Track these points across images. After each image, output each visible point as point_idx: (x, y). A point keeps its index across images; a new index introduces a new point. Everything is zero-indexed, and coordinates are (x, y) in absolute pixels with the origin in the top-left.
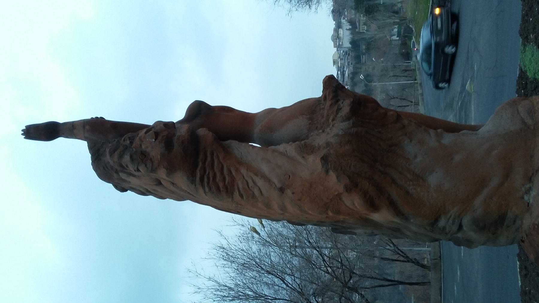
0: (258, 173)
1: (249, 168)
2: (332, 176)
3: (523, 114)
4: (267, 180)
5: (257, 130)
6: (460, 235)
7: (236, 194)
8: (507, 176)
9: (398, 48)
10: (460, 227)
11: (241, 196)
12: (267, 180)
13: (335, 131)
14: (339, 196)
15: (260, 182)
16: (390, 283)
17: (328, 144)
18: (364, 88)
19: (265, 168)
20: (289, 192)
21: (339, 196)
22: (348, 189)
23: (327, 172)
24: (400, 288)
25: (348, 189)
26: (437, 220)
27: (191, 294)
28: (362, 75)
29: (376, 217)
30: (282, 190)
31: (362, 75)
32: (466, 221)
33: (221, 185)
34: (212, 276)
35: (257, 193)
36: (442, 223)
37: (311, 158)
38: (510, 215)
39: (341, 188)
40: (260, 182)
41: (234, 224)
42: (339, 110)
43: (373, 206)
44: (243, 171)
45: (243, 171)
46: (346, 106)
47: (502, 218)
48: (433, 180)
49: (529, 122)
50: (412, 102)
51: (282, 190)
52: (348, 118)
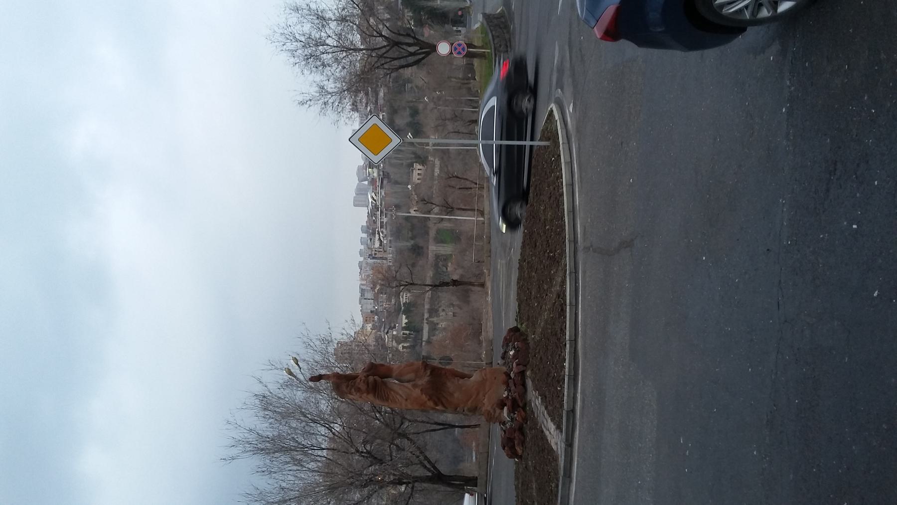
0: (398, 393)
1: (394, 391)
2: (424, 396)
3: (483, 375)
4: (401, 396)
5: (394, 375)
6: (464, 413)
7: (390, 401)
8: (478, 394)
9: (461, 69)
10: (464, 411)
11: (391, 401)
12: (401, 396)
13: (425, 380)
14: (426, 402)
15: (398, 397)
16: (441, 427)
17: (422, 384)
18: (409, 119)
19: (400, 392)
20: (409, 401)
21: (426, 402)
22: (429, 400)
23: (422, 394)
24: (456, 432)
25: (429, 400)
26: (457, 409)
27: (341, 438)
28: (409, 134)
29: (437, 408)
30: (406, 400)
31: (409, 134)
32: (466, 409)
33: (384, 398)
34: (253, 427)
35: (397, 401)
36: (458, 409)
37: (417, 389)
38: (478, 407)
39: (426, 399)
40: (398, 397)
41: (271, 368)
42: (426, 374)
43: (436, 404)
44: (392, 393)
45: (392, 393)
46: (428, 372)
47: (476, 407)
48: (456, 395)
49: (485, 378)
50: (476, 184)
51: (406, 400)
52: (429, 376)
